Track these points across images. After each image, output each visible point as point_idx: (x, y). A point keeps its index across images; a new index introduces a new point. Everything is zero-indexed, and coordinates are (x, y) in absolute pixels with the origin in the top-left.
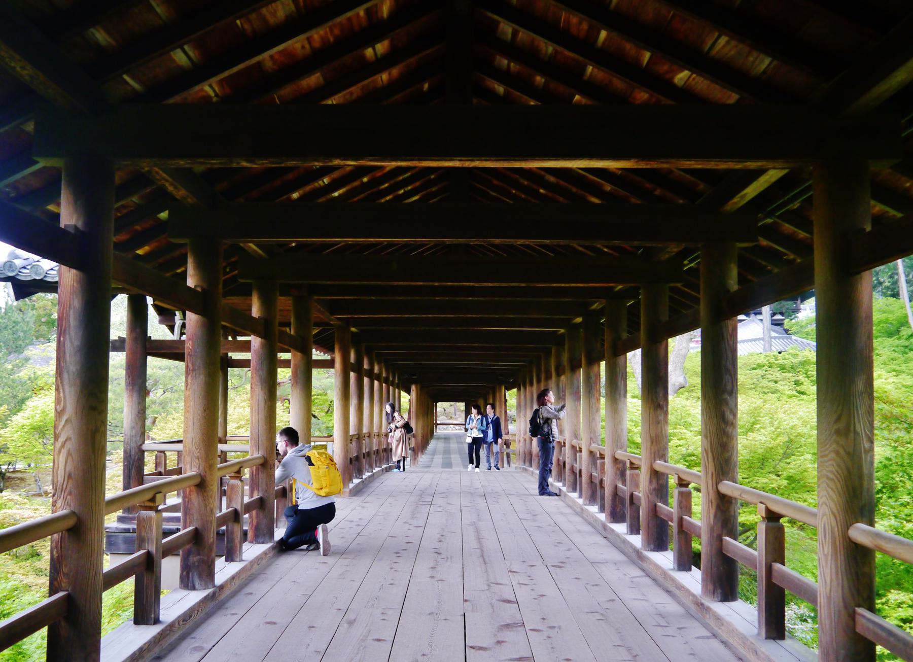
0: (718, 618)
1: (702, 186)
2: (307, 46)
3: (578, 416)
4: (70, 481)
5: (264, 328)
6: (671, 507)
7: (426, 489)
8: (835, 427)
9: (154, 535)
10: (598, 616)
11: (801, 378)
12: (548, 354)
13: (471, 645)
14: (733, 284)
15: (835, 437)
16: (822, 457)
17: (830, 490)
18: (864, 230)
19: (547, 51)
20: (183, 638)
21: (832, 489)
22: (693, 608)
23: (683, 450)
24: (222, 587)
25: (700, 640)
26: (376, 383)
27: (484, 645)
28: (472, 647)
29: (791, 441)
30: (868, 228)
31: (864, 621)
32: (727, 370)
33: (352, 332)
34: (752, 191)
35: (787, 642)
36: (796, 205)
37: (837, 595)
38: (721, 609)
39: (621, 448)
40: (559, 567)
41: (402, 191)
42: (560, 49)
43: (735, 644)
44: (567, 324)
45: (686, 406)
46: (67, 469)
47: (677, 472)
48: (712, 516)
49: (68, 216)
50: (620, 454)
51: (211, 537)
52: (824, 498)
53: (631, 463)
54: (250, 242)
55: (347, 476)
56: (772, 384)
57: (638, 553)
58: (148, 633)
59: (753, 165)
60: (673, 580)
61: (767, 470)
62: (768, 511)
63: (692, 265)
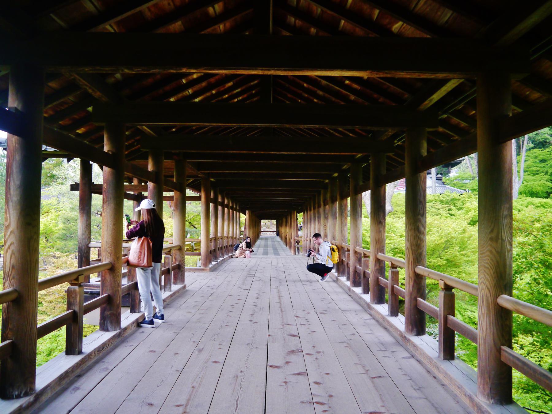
0: (414, 346)
1: (407, 96)
2: (172, 4)
3: (335, 227)
4: (14, 270)
5: (155, 177)
6: (386, 281)
7: (252, 267)
8: (490, 236)
9: (78, 301)
10: (345, 344)
11: (452, 207)
12: (319, 194)
13: (270, 364)
14: (424, 153)
15: (489, 242)
16: (481, 254)
17: (486, 274)
18: (509, 115)
19: (317, 12)
20: (97, 362)
21: (488, 274)
22: (400, 338)
23: (392, 246)
24: (125, 329)
25: (405, 359)
26: (226, 209)
27: (278, 365)
28: (271, 366)
29: (448, 241)
30: (511, 115)
31: (507, 354)
32: (421, 202)
33: (211, 181)
34: (436, 97)
35: (456, 362)
36: (460, 107)
37: (490, 339)
38: (416, 340)
39: (359, 245)
40: (324, 314)
41: (236, 100)
42: (325, 9)
43: (425, 362)
44: (330, 177)
45: (397, 224)
46: (12, 263)
47: (390, 260)
48: (411, 286)
49: (13, 103)
50: (358, 249)
51: (118, 300)
52: (482, 279)
53: (364, 254)
54: (144, 125)
55: (208, 261)
56: (436, 211)
57: (368, 305)
58: (75, 359)
59: (441, 76)
60: (388, 322)
61: (436, 256)
62: (446, 285)
63: (399, 143)
